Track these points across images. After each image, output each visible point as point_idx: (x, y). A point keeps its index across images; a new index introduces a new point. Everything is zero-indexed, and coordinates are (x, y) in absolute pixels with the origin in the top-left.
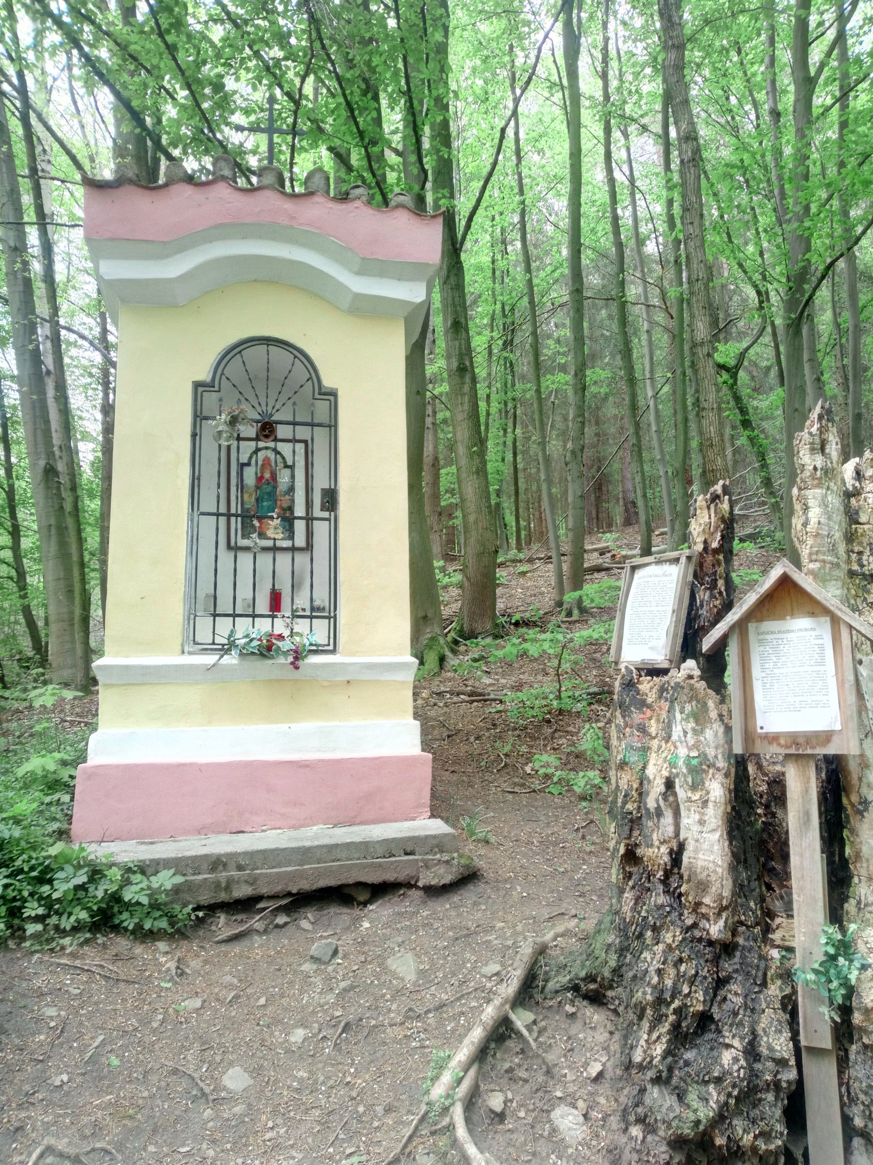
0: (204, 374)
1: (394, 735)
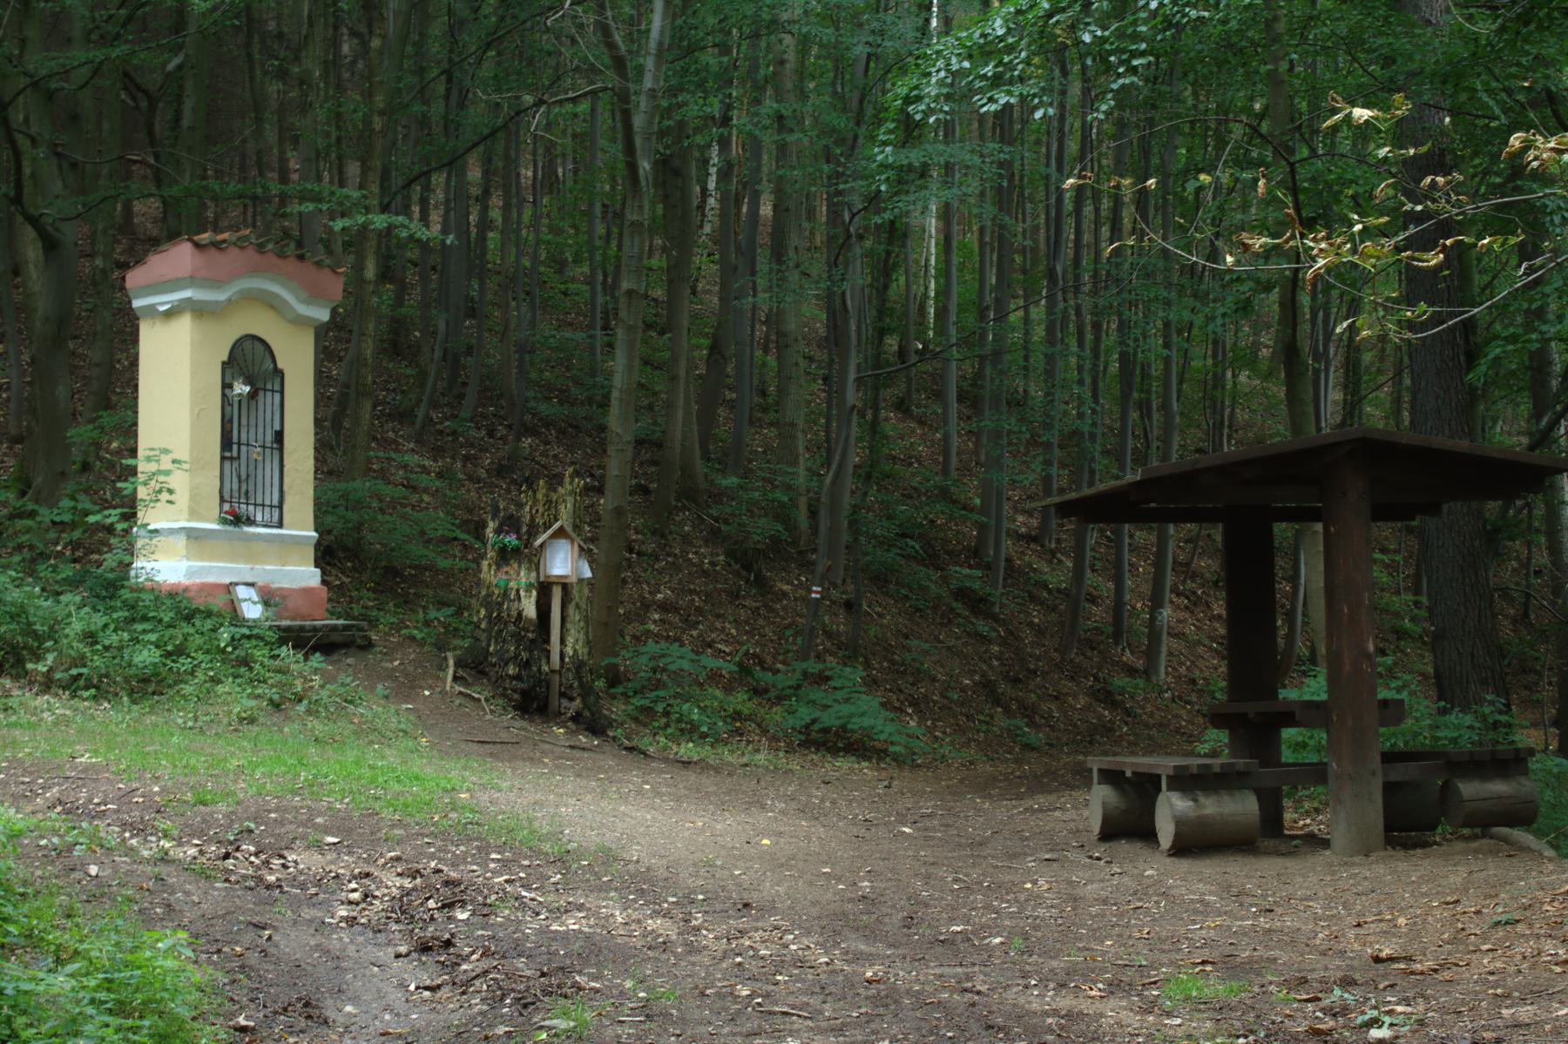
0: (225, 358)
1: (304, 574)
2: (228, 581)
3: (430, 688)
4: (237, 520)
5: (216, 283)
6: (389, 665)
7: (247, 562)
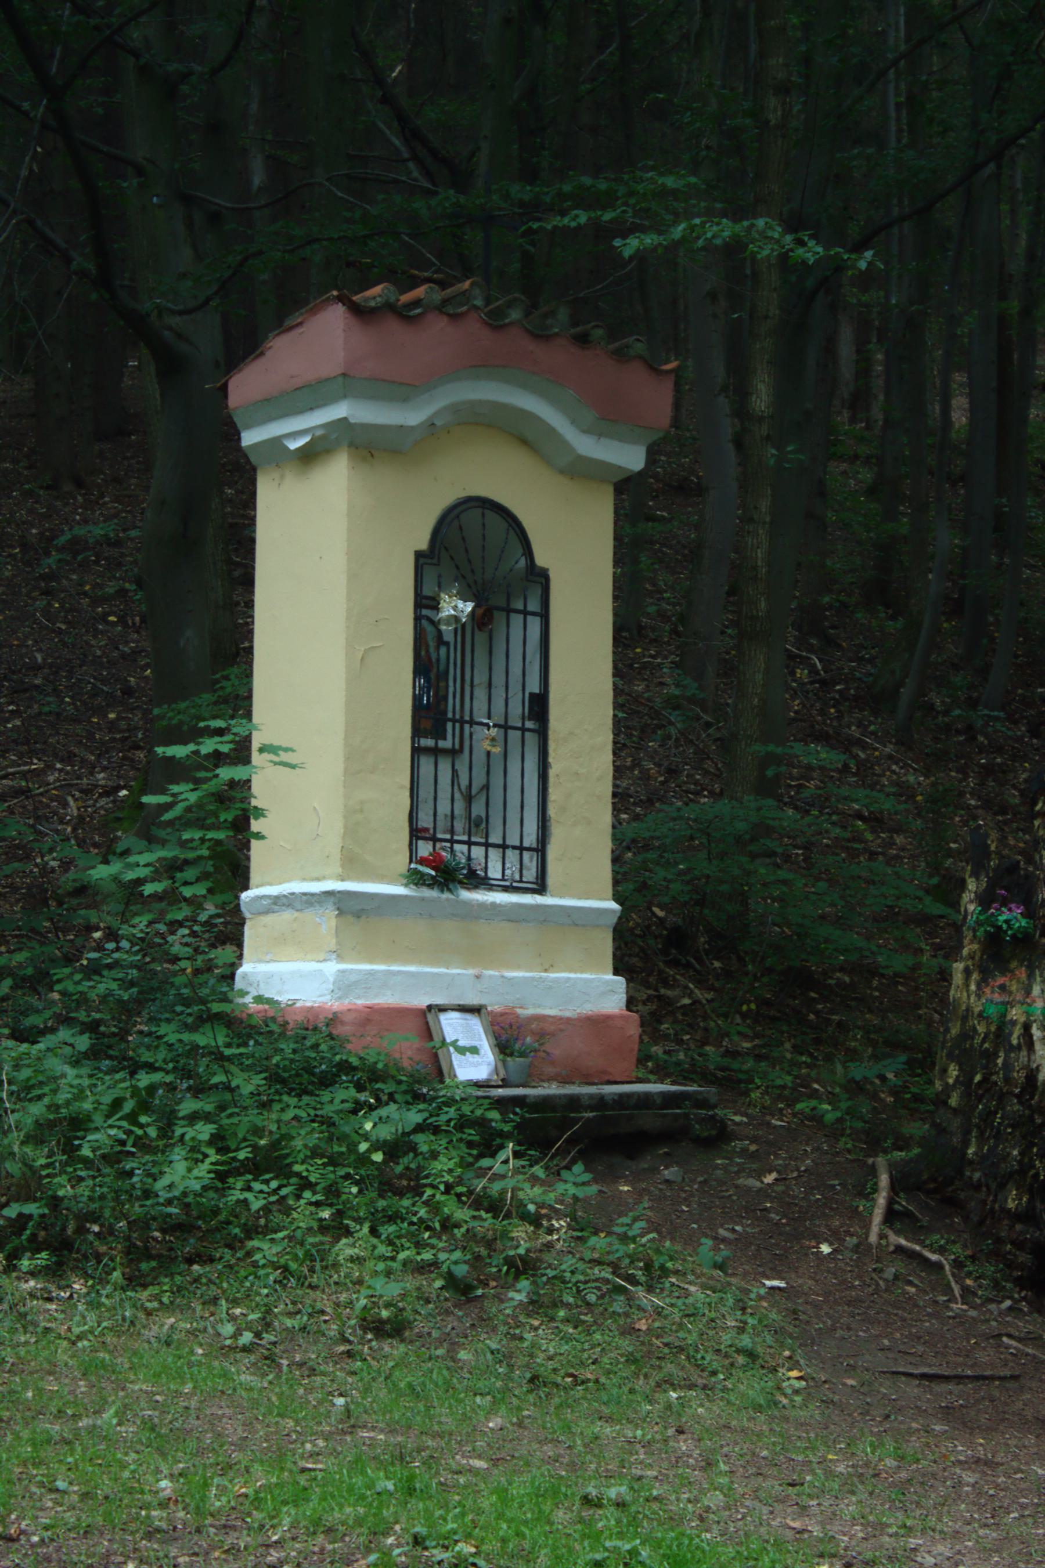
0: (423, 545)
1: (589, 988)
2: (422, 1001)
3: (835, 1237)
4: (446, 876)
5: (400, 389)
6: (753, 1183)
7: (466, 965)
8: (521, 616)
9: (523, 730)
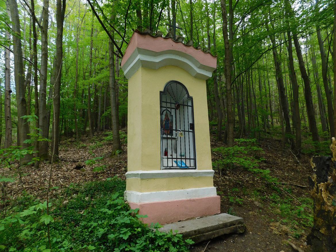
0: (162, 90)
1: (209, 191)
8: (186, 158)
9: (189, 132)
